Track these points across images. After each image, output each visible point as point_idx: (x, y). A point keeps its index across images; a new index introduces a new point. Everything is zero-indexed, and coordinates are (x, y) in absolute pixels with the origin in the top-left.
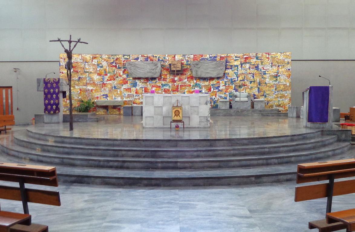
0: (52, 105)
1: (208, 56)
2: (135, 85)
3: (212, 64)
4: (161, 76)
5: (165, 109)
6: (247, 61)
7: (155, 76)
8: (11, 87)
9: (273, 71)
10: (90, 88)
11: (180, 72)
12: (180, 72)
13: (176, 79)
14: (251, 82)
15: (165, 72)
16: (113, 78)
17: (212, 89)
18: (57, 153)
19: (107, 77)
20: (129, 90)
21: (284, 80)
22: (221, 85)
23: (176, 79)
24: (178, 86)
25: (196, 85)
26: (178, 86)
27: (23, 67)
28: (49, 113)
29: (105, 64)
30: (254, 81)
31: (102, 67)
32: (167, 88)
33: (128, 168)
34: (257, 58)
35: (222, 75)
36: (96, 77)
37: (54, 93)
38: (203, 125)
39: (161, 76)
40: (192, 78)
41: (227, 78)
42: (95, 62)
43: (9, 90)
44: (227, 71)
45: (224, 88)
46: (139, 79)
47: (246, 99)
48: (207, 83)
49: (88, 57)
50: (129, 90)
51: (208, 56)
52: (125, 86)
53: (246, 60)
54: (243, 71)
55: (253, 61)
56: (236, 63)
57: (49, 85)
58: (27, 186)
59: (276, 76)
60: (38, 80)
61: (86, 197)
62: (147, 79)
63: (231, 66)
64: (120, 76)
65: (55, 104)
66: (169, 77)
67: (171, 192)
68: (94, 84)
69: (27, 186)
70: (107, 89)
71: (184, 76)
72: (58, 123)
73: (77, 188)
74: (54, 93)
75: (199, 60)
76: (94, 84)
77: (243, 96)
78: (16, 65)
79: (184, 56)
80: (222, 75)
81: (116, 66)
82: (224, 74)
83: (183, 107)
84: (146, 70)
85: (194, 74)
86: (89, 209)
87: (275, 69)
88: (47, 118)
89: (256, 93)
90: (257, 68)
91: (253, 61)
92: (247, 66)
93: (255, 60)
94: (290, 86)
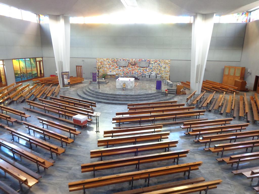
0: (94, 76)
1: (144, 60)
2: (120, 68)
3: (144, 63)
4: (128, 66)
5: (121, 84)
6: (156, 62)
7: (126, 66)
8: (82, 66)
9: (164, 66)
10: (106, 69)
11: (135, 64)
12: (135, 64)
13: (133, 67)
14: (157, 69)
15: (129, 65)
16: (113, 66)
17: (145, 71)
18: (96, 95)
19: (111, 66)
20: (118, 70)
21: (168, 69)
22: (147, 70)
23: (133, 67)
24: (133, 69)
25: (139, 69)
26: (133, 69)
27: (85, 60)
28: (94, 81)
29: (110, 61)
30: (158, 69)
31: (109, 62)
32: (130, 70)
33: (109, 100)
34: (159, 61)
35: (147, 66)
36: (108, 66)
37: (95, 76)
38: (131, 88)
39: (128, 66)
40: (138, 67)
41: (149, 67)
42: (107, 61)
43: (81, 67)
44: (150, 65)
45: (148, 70)
46: (121, 66)
47: (154, 75)
48: (143, 69)
49: (105, 59)
50: (118, 70)
51: (144, 60)
52: (117, 69)
53: (156, 62)
54: (155, 65)
55: (158, 62)
56: (152, 62)
57: (94, 74)
58: (92, 104)
59: (165, 68)
60: (91, 73)
61: (101, 105)
62: (124, 67)
63: (151, 63)
64: (115, 65)
65: (95, 79)
66: (131, 66)
67: (4, 136)
68: (107, 68)
69: (92, 104)
70: (111, 70)
71: (136, 66)
72: (96, 84)
73: (99, 104)
74: (95, 76)
75: (141, 61)
76: (107, 68)
77: (154, 74)
78: (83, 59)
79: (136, 59)
80: (147, 66)
81: (114, 62)
82: (149, 66)
83: (126, 84)
84: (123, 64)
85: (139, 66)
86: (101, 108)
87: (165, 65)
88: (93, 83)
89: (159, 73)
90: (159, 64)
91: (158, 62)
92: (156, 63)
93: (159, 62)
94: (169, 71)
